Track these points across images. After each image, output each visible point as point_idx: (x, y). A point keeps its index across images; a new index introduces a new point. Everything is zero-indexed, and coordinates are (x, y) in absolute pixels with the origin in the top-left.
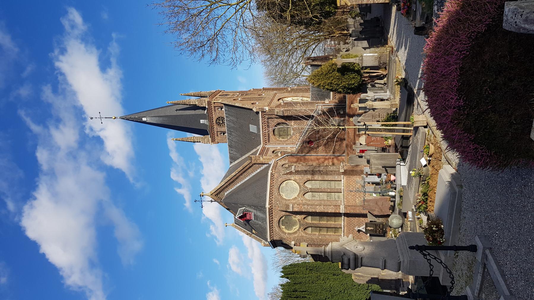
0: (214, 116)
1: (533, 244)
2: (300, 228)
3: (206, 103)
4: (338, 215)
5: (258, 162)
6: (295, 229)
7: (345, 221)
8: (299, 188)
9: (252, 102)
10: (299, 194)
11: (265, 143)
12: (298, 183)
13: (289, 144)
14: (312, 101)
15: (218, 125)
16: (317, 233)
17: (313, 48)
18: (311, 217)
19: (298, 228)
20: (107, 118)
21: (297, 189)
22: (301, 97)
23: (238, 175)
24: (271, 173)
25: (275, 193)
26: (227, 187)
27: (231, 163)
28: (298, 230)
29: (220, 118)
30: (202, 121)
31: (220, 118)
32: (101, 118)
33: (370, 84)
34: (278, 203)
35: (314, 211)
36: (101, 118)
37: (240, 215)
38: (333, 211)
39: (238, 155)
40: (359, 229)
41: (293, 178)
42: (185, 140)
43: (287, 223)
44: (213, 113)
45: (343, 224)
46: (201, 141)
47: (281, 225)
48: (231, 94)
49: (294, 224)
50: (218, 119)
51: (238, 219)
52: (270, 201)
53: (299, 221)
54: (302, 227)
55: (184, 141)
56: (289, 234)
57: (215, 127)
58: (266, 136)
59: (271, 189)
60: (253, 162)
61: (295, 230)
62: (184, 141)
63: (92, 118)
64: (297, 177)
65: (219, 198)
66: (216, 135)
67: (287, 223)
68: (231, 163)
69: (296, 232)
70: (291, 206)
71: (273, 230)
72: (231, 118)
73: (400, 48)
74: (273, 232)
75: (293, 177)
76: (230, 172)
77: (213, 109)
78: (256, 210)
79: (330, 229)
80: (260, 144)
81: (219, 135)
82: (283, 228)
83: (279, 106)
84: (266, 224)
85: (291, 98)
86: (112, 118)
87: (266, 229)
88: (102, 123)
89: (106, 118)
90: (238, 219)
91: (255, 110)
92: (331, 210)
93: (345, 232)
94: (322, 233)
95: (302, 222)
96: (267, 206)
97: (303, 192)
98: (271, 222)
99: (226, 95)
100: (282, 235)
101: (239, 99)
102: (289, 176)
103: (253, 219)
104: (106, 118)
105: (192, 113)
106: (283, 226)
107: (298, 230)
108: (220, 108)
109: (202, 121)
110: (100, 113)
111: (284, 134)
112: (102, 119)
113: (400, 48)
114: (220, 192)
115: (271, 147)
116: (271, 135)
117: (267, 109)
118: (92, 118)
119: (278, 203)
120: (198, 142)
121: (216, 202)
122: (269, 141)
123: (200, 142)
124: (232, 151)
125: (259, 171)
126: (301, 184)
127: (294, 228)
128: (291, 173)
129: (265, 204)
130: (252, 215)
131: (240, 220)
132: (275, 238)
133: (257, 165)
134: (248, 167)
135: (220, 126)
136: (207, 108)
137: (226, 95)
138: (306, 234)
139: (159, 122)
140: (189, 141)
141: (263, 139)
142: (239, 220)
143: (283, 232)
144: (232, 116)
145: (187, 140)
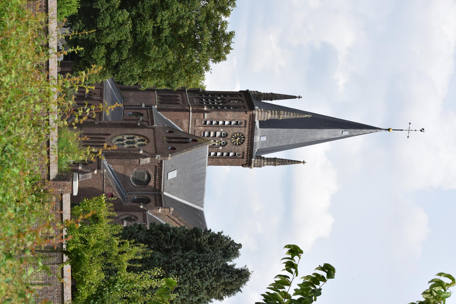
0: (246, 147)
15: (242, 135)
20: (401, 130)
29: (239, 145)
31: (239, 144)
32: (409, 130)
33: (6, 170)
36: (409, 130)
44: (246, 150)
50: (242, 143)
57: (247, 133)
63: (421, 131)
73: (113, 90)
77: (245, 155)
80: (133, 181)
81: (244, 122)
86: (394, 130)
89: (402, 130)
104: (402, 130)
105: (277, 101)
107: (32, 19)
108: (237, 155)
113: (113, 90)
118: (421, 131)
121: (238, 244)
135: (240, 134)
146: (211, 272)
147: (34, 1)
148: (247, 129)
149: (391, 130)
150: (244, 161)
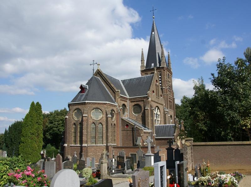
1: (196, 186)
4: (81, 142)
5: (116, 96)
8: (98, 119)
9: (155, 91)
10: (94, 120)
11: (130, 99)
12: (101, 119)
13: (130, 113)
14: (154, 127)
16: (73, 131)
21: (97, 118)
22: (161, 120)
24: (107, 103)
25: (95, 106)
26: (103, 78)
27: (122, 81)
30: (153, 65)
35: (84, 129)
38: (83, 140)
39: (125, 84)
41: (104, 116)
48: (170, 80)
49: (77, 118)
52: (89, 103)
56: (72, 115)
59: (97, 103)
60: (116, 93)
61: (74, 118)
64: (105, 119)
66: (145, 73)
68: (122, 81)
70: (86, 115)
72: (146, 79)
75: (104, 116)
76: (116, 82)
78: (86, 95)
79: (75, 137)
82: (155, 114)
83: (151, 107)
85: (160, 114)
87: (75, 102)
91: (149, 92)
92: (84, 138)
94: (73, 134)
96: (86, 102)
97: (95, 122)
99: (169, 77)
101: (157, 83)
102: (105, 114)
107: (74, 120)
109: (153, 65)
111: (136, 110)
114: (99, 74)
115: (128, 104)
116: (135, 103)
117: (150, 99)
122: (131, 102)
124: (128, 81)
125: (111, 96)
126: (100, 121)
127: (76, 117)
128: (107, 115)
129: (87, 100)
133: (114, 95)
137: (169, 77)
144: (147, 79)
148: (148, 72)
150: (162, 70)
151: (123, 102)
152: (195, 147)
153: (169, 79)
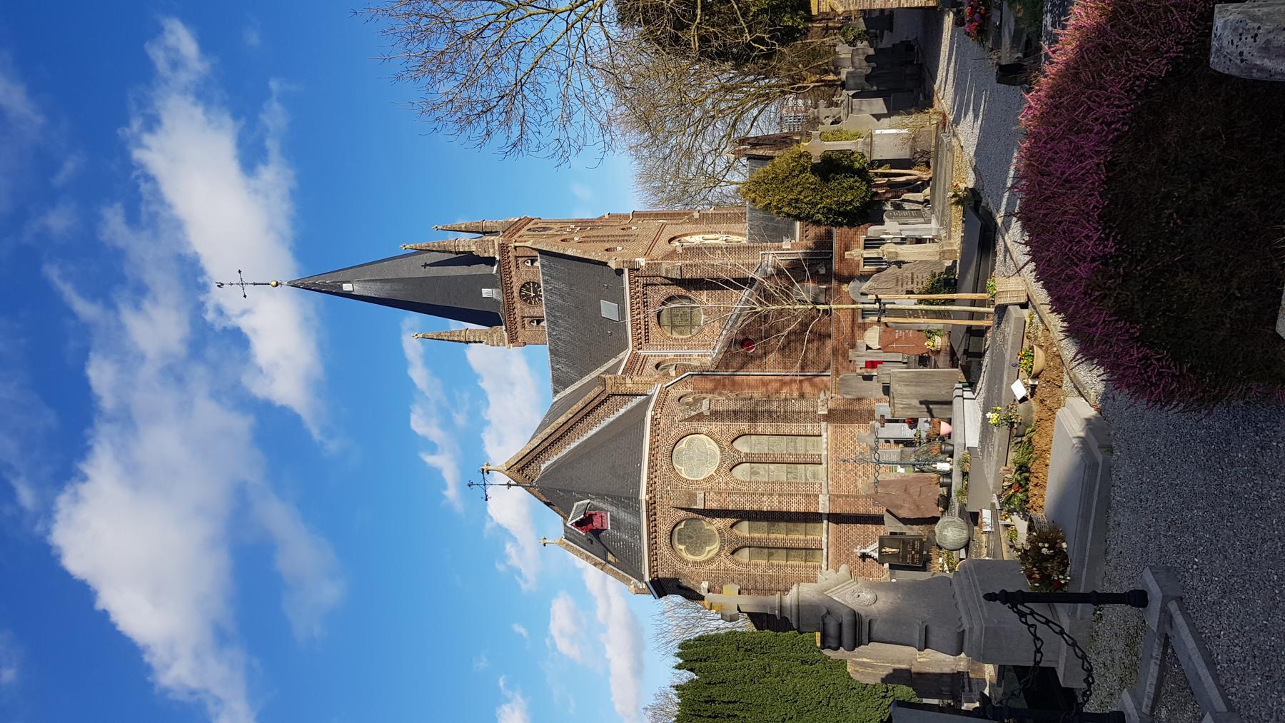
0: (514, 279)
2: (721, 548)
3: (497, 248)
4: (814, 518)
5: (622, 390)
6: (709, 551)
7: (830, 533)
8: (718, 453)
9: (607, 246)
10: (720, 467)
11: (639, 345)
12: (716, 441)
13: (695, 347)
14: (752, 244)
16: (763, 562)
17: (754, 115)
18: (747, 522)
19: (717, 550)
20: (257, 284)
21: (714, 457)
22: (725, 233)
23: (573, 421)
24: (652, 417)
25: (663, 465)
26: (545, 450)
27: (556, 392)
28: (717, 554)
29: (528, 283)
30: (486, 292)
31: (529, 284)
32: (242, 284)
34: (669, 488)
36: (242, 284)
37: (578, 519)
38: (802, 509)
39: (573, 374)
40: (863, 551)
41: (704, 430)
42: (445, 338)
43: (690, 537)
44: (513, 273)
45: (824, 540)
46: (484, 339)
47: (677, 543)
48: (557, 227)
49: (708, 540)
50: (523, 286)
51: (573, 528)
52: (650, 485)
53: (720, 534)
54: (726, 548)
55: (443, 340)
56: (696, 563)
57: (518, 306)
58: (640, 328)
59: (651, 455)
60: (609, 391)
61: (711, 555)
62: (443, 340)
63: (223, 285)
64: (715, 427)
65: (528, 477)
66: (519, 325)
67: (690, 537)
68: (556, 392)
69: (713, 558)
71: (656, 554)
72: (557, 285)
73: (963, 115)
74: (656, 558)
75: (704, 427)
76: (553, 413)
77: (513, 263)
78: (616, 506)
79: (793, 553)
81: (526, 325)
84: (640, 539)
85: (701, 236)
86: (268, 284)
87: (640, 551)
88: (245, 296)
89: (255, 284)
90: (573, 528)
92: (796, 506)
93: (830, 558)
94: (775, 562)
95: (726, 535)
96: (643, 496)
97: (728, 463)
98: (652, 534)
99: (545, 229)
100: (679, 565)
101: (576, 239)
102: (696, 424)
103: (609, 528)
104: (255, 284)
105: (462, 273)
106: (681, 544)
107: (718, 554)
108: (529, 261)
109: (486, 292)
110: (240, 272)
111: (684, 323)
112: (246, 287)
113: (963, 115)
114: (529, 463)
116: (651, 325)
117: (642, 262)
118: (223, 285)
119: (669, 488)
120: (475, 342)
121: (521, 487)
122: (647, 340)
123: (481, 342)
124: (558, 363)
125: (622, 411)
126: (725, 444)
127: (708, 548)
128: (700, 417)
129: (638, 493)
130: (607, 518)
131: (577, 530)
132: (662, 574)
133: (619, 398)
134: (596, 402)
136: (499, 261)
137: (545, 229)
138: (737, 563)
139: (383, 295)
140: (456, 339)
141: (632, 335)
142: (576, 529)
143: (682, 560)
144: (558, 279)
145: (450, 338)
146: (1198, 54)
147: (1254, 2)
149: (274, 283)
151: (649, 367)
152: (847, 527)
153: (550, 229)
